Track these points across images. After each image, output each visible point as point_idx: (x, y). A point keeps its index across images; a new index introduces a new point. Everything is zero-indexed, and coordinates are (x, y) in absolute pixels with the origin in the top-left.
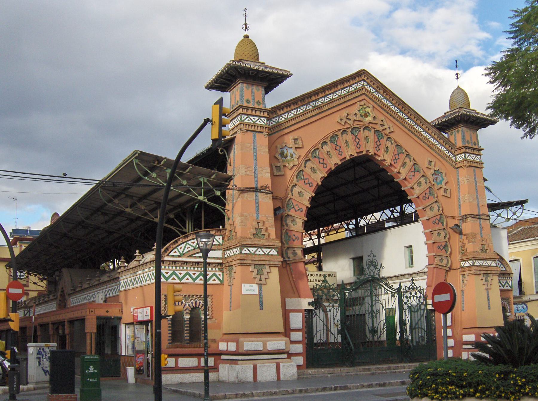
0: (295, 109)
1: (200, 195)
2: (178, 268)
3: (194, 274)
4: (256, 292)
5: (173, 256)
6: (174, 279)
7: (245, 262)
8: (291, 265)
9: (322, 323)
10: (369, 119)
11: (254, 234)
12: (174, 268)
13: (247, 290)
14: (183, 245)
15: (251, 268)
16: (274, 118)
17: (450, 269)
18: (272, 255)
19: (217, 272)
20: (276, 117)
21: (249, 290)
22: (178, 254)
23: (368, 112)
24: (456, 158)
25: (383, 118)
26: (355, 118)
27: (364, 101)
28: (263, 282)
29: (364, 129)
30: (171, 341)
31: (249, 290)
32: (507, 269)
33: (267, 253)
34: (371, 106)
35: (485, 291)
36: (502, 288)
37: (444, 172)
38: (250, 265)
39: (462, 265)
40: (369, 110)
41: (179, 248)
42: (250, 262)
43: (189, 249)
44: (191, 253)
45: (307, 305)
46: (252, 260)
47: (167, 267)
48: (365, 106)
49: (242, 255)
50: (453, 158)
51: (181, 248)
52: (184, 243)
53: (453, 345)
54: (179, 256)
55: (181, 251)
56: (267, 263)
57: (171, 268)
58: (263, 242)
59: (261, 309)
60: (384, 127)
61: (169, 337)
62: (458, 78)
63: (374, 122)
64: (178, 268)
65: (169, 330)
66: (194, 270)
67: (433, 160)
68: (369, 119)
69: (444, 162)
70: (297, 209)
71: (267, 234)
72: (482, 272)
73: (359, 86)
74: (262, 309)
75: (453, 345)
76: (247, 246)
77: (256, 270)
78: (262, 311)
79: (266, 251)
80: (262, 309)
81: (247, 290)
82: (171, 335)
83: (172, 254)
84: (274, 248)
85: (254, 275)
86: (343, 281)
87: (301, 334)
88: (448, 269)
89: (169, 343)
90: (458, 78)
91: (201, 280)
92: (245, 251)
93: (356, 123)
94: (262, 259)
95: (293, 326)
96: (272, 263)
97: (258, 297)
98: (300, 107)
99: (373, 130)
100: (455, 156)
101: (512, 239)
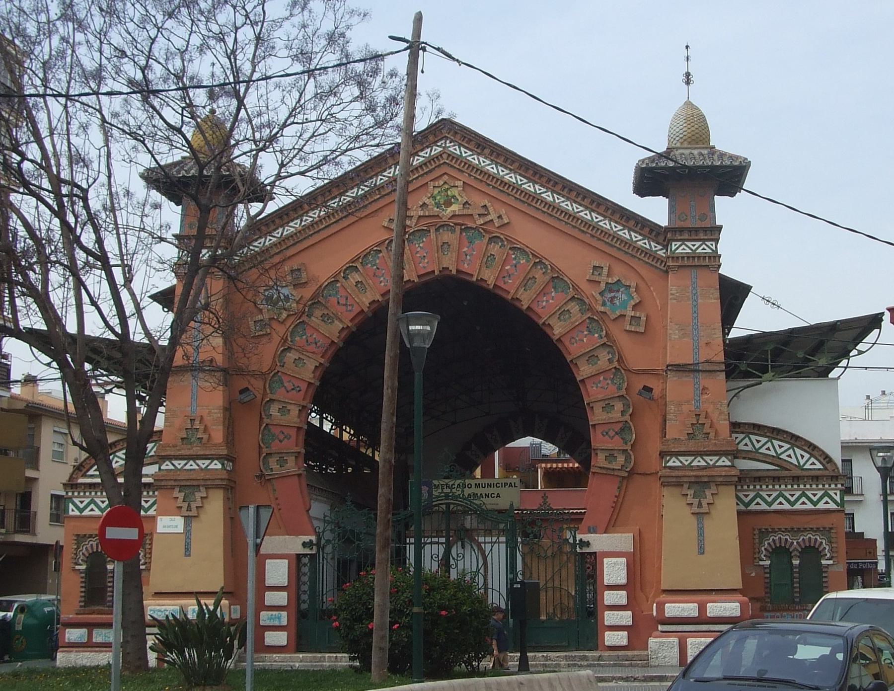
0: (297, 218)
2: (99, 494)
3: (769, 496)
4: (181, 529)
6: (92, 510)
7: (163, 483)
8: (274, 482)
9: (496, 587)
10: (455, 208)
11: (182, 439)
12: (93, 494)
13: (164, 527)
15: (176, 493)
16: (256, 240)
17: (632, 473)
19: (762, 490)
20: (260, 237)
21: (169, 527)
23: (454, 197)
25: (486, 202)
26: (421, 213)
27: (446, 178)
28: (705, 509)
29: (437, 230)
30: (83, 604)
31: (169, 527)
32: (828, 466)
33: (203, 467)
34: (460, 183)
35: (693, 519)
36: (742, 507)
37: (633, 284)
38: (173, 488)
40: (454, 192)
42: (173, 483)
45: (301, 546)
46: (175, 480)
47: (82, 494)
48: (447, 186)
49: (162, 473)
53: (630, 623)
56: (202, 483)
57: (87, 494)
58: (197, 450)
60: (489, 218)
61: (82, 597)
63: (465, 212)
64: (99, 494)
65: (82, 587)
67: (605, 263)
68: (455, 208)
69: (634, 263)
70: (289, 389)
71: (205, 437)
72: (685, 479)
73: (437, 150)
74: (189, 555)
75: (630, 623)
76: (170, 458)
77: (181, 496)
79: (204, 464)
80: (189, 555)
81: (164, 527)
82: (83, 594)
84: (217, 459)
85: (179, 502)
87: (285, 594)
88: (626, 474)
89: (81, 606)
92: (167, 466)
93: (424, 222)
94: (191, 477)
95: (269, 582)
96: (209, 483)
97: (183, 537)
98: (307, 212)
99: (458, 228)
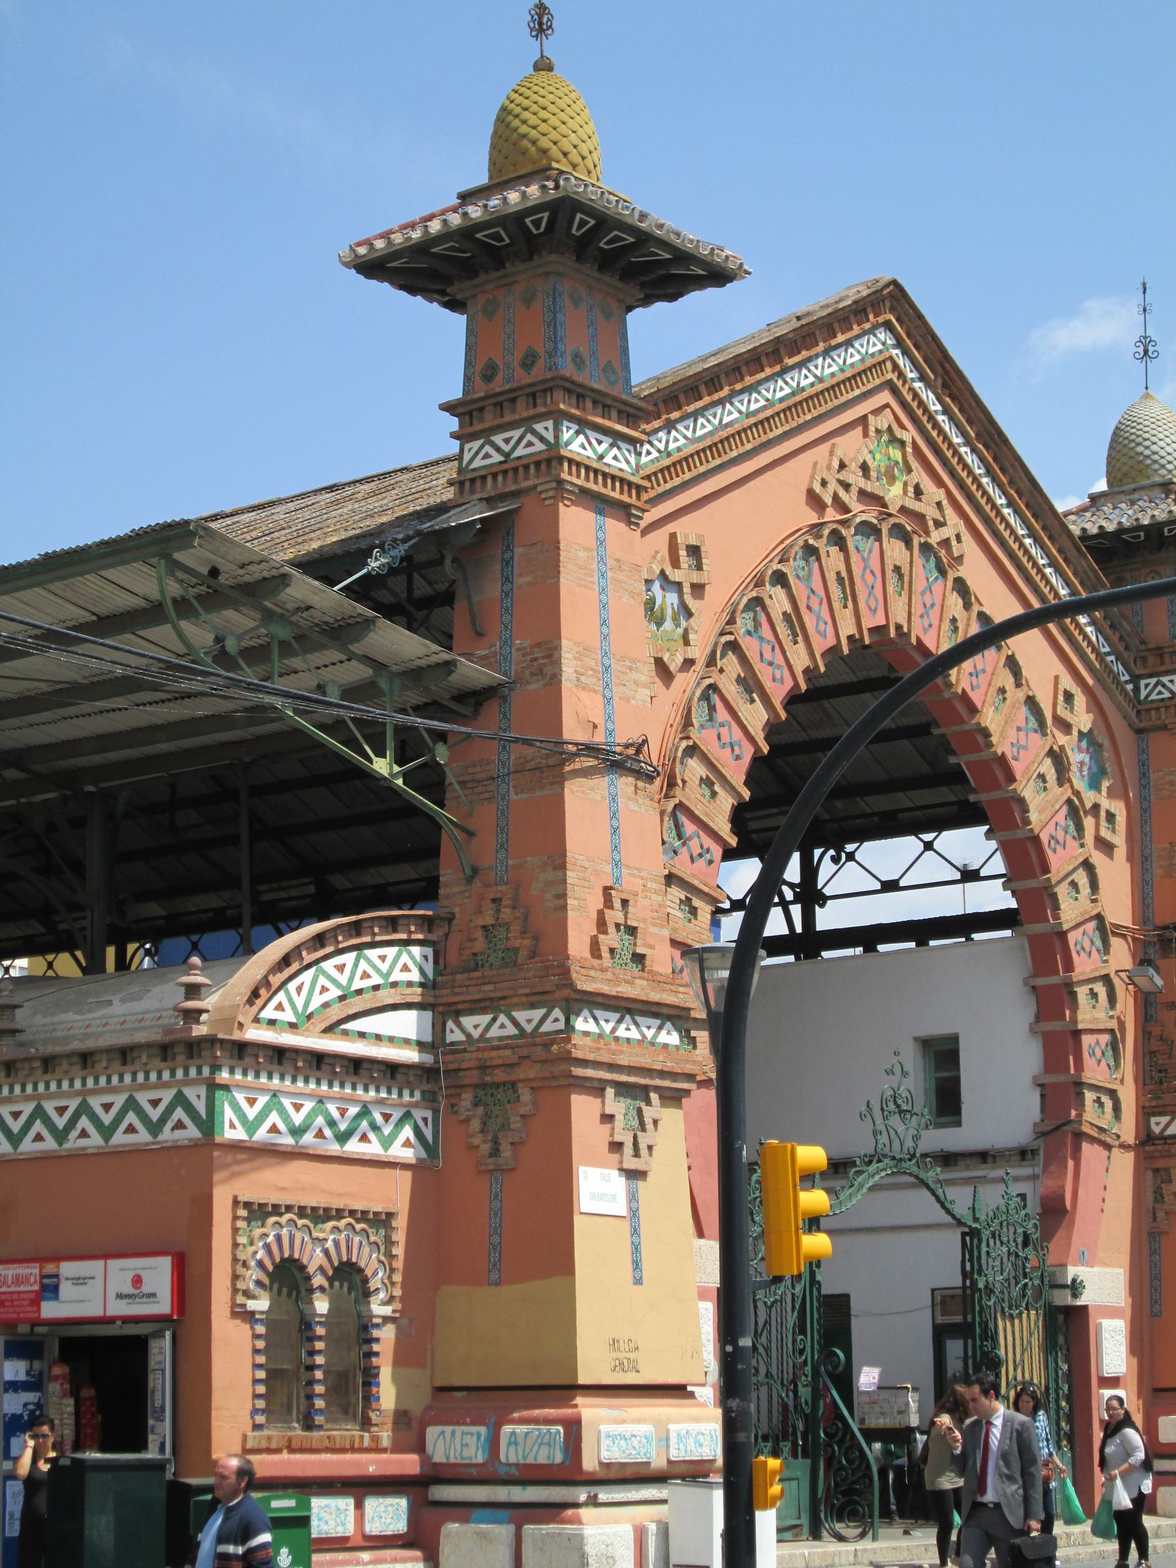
1: (381, 754)
4: (620, 1207)
5: (272, 1022)
14: (307, 976)
18: (533, 1006)
22: (288, 1016)
24: (1137, 690)
39: (1157, 1130)
41: (292, 986)
43: (327, 997)
44: (337, 1012)
50: (1130, 687)
51: (299, 989)
52: (309, 966)
54: (293, 1026)
55: (300, 1002)
59: (638, 1281)
62: (1144, 285)
66: (110, 1090)
78: (639, 1287)
83: (268, 1013)
86: (448, 408)
90: (1144, 285)
91: (1157, 1124)
100: (1135, 679)
101: (334, 1240)
